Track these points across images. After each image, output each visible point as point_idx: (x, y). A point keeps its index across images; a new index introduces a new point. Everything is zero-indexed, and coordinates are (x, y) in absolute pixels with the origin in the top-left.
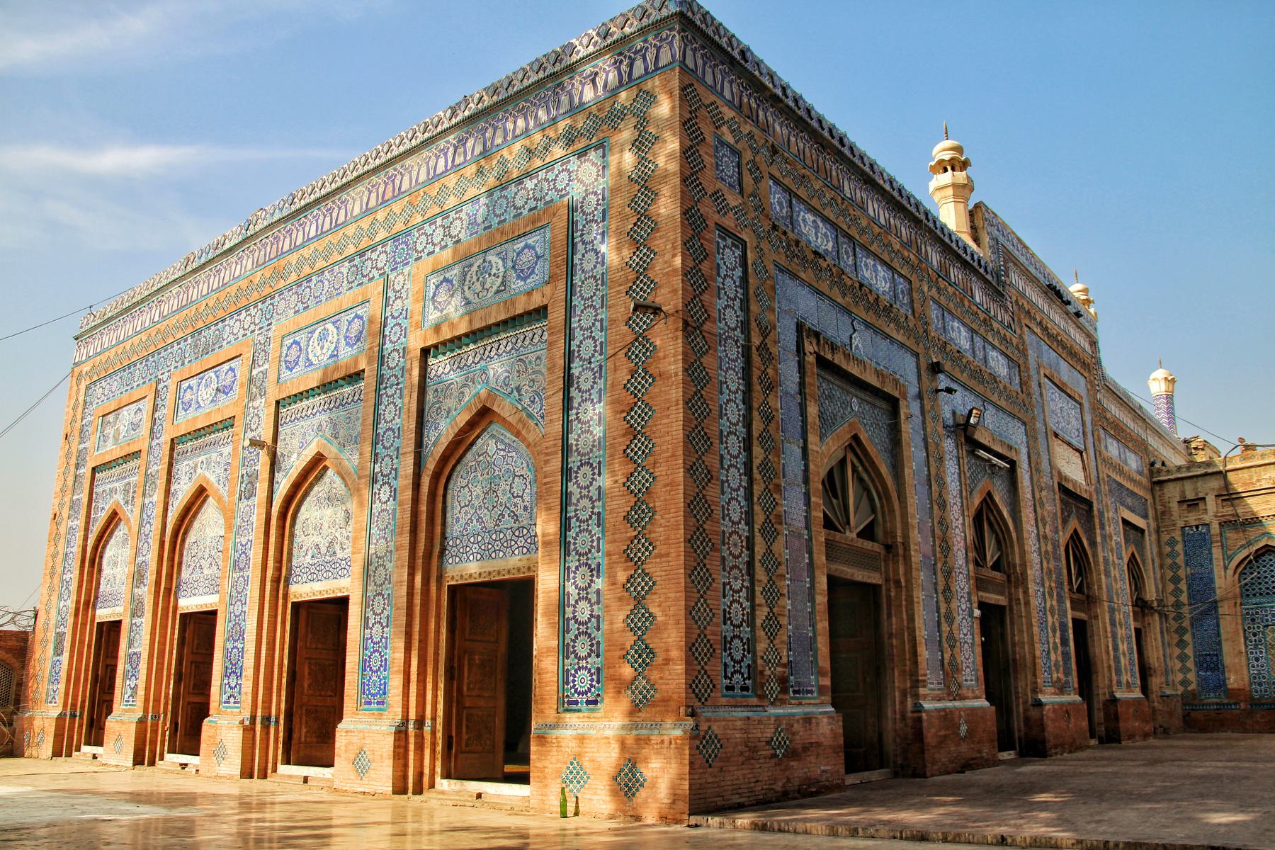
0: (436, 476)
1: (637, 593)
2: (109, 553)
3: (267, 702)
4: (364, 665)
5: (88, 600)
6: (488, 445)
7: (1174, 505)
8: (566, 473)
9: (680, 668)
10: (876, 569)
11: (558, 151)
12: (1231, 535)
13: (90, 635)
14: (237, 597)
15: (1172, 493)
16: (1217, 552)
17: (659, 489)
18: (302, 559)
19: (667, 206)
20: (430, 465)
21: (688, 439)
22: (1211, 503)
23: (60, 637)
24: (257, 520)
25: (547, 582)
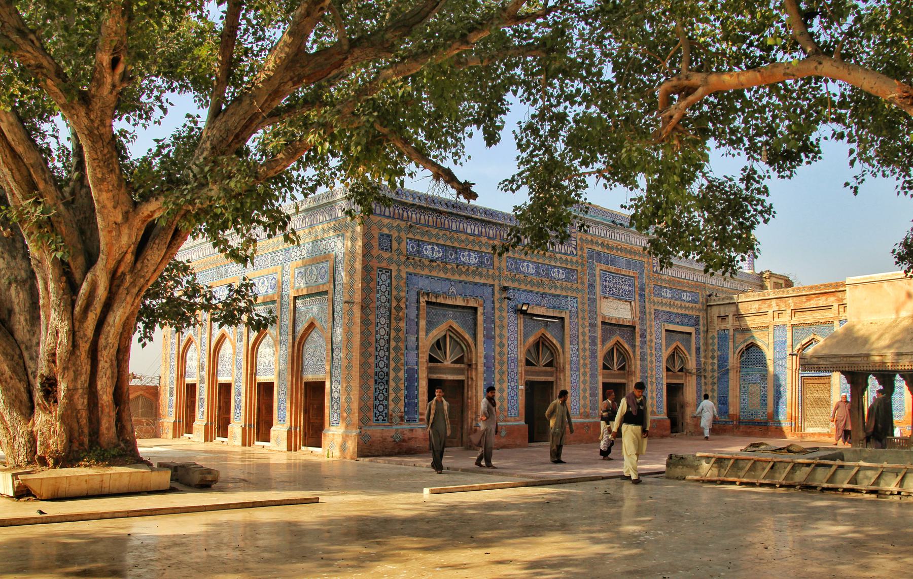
0: (299, 343)
1: (348, 390)
2: (189, 354)
3: (250, 421)
4: (279, 408)
5: (182, 375)
6: (314, 335)
7: (715, 318)
8: (332, 350)
9: (357, 415)
10: (463, 374)
11: (331, 233)
12: (738, 336)
13: (184, 389)
14: (238, 380)
15: (715, 312)
16: (731, 344)
17: (354, 359)
18: (260, 367)
19: (358, 266)
20: (297, 340)
21: (362, 344)
22: (730, 318)
23: (171, 389)
24: (244, 350)
25: (327, 385)
